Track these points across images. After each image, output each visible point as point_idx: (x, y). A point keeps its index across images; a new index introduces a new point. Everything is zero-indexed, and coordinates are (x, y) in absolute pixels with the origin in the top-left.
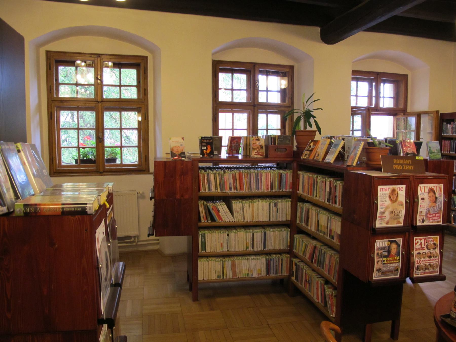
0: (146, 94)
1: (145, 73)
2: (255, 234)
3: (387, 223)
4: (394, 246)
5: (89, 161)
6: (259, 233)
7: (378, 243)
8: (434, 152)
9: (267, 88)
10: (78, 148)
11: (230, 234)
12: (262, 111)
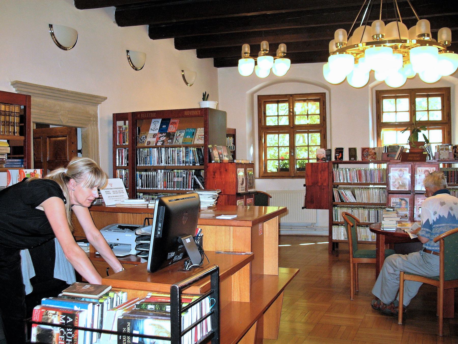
0: (325, 120)
2: (370, 211)
3: (398, 188)
4: (403, 202)
5: (287, 170)
6: (372, 212)
7: (393, 199)
11: (353, 211)
12: (317, 131)
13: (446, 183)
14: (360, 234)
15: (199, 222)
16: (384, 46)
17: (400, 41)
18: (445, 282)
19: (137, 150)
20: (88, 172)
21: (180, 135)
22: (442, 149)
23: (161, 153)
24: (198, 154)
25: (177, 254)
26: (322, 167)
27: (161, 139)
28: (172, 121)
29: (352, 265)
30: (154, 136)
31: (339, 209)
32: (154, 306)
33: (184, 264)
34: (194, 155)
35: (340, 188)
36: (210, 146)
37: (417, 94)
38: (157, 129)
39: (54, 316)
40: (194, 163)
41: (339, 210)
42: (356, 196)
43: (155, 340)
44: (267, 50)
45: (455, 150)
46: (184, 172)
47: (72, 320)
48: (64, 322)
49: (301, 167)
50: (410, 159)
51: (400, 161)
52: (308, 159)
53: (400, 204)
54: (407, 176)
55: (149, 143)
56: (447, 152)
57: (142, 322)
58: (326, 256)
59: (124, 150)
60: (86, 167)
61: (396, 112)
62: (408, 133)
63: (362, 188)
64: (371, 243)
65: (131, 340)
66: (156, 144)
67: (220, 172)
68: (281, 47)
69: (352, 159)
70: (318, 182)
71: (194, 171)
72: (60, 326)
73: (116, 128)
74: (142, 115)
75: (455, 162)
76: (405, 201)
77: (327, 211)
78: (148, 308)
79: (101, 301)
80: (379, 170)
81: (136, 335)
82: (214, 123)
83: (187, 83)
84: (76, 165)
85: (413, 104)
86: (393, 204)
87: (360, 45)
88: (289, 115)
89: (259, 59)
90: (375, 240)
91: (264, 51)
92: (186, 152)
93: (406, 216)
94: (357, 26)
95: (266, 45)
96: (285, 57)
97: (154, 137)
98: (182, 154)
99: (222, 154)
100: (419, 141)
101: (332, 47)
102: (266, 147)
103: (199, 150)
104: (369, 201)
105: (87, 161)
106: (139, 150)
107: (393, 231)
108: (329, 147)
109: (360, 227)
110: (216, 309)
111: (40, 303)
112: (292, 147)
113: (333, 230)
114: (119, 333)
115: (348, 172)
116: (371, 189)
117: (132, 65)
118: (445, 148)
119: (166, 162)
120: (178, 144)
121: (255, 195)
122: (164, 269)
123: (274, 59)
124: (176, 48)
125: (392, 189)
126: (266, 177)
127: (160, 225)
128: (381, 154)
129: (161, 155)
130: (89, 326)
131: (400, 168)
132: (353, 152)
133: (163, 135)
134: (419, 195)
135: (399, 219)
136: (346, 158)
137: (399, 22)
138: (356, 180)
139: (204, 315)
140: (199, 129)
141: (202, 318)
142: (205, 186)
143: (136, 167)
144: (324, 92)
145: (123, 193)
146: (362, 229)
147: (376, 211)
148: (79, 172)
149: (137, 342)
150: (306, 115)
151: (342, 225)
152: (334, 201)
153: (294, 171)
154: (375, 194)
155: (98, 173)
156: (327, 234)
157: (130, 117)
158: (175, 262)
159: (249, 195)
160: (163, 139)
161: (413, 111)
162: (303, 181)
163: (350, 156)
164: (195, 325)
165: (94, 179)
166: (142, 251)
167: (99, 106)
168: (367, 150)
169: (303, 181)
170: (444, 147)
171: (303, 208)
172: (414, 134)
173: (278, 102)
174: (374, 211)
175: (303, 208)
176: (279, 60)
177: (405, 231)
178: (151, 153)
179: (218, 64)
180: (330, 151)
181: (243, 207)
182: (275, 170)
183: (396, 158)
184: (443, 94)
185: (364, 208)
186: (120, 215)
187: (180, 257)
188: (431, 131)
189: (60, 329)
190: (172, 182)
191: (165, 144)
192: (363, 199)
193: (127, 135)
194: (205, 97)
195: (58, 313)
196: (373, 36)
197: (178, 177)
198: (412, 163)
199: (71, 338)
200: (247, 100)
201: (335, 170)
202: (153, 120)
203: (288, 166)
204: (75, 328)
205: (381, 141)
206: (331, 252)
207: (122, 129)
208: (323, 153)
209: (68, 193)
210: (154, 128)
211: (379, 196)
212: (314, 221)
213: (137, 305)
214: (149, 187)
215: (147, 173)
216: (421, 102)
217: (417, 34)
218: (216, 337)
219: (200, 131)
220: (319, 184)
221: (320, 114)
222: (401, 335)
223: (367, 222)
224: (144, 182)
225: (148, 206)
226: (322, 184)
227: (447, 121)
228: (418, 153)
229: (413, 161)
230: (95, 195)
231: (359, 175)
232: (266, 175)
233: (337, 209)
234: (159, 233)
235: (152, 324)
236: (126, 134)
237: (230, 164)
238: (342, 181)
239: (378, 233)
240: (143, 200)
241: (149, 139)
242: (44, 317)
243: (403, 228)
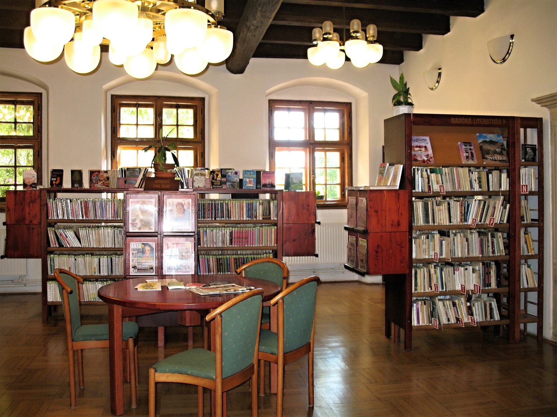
1: (39, 110)
2: (101, 259)
3: (140, 229)
4: (147, 248)
6: (104, 260)
8: (296, 183)
9: (15, 119)
11: (77, 259)
14: (87, 292)
26: (31, 197)
31: (57, 258)
42: (81, 239)
45: (213, 175)
51: (142, 189)
54: (153, 208)
56: (202, 178)
58: (38, 326)
62: (151, 153)
69: (75, 185)
70: (24, 219)
75: (211, 192)
76: (150, 246)
77: (39, 261)
85: (158, 115)
86: (133, 252)
93: (152, 268)
100: (167, 162)
104: (100, 245)
113: (48, 287)
115: (69, 205)
116: (102, 228)
118: (201, 173)
128: (116, 180)
131: (142, 200)
132: (77, 175)
136: (67, 184)
138: (81, 215)
144: (40, 92)
147: (109, 260)
150: (13, 123)
152: (49, 246)
161: (158, 125)
168: (96, 173)
184: (196, 106)
198: (160, 193)
201: (50, 202)
205: (117, 163)
211: (113, 238)
212: (23, 273)
216: (168, 115)
220: (27, 222)
226: (31, 221)
227: (200, 140)
228: (166, 178)
229: (160, 189)
231: (85, 208)
238: (60, 217)
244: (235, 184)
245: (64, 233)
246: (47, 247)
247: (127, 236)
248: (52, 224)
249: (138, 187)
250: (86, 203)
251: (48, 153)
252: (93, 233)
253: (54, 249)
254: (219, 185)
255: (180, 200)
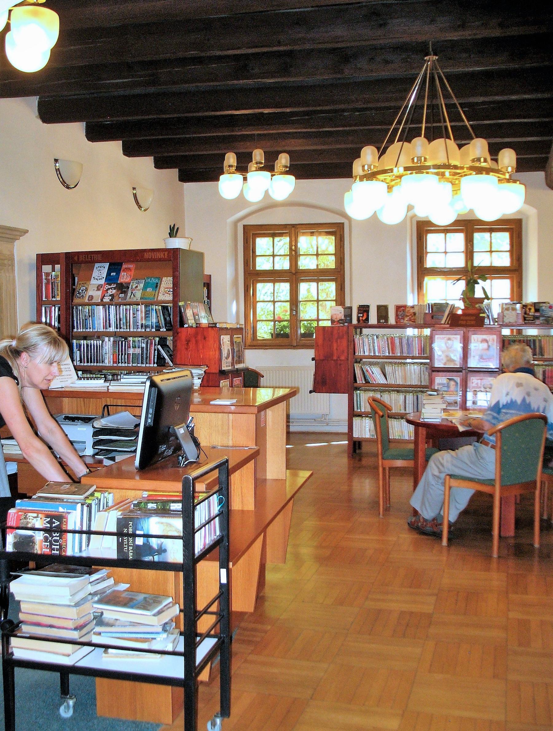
0: (343, 263)
1: (341, 241)
2: (407, 396)
4: (452, 383)
5: (286, 336)
6: (410, 397)
10: (274, 321)
13: (531, 356)
15: (192, 408)
16: (427, 173)
17: (447, 166)
18: (502, 487)
19: (73, 308)
20: (46, 343)
21: (137, 287)
22: (507, 309)
23: (109, 312)
24: (163, 315)
25: (169, 448)
27: (110, 292)
28: (124, 266)
29: (381, 469)
30: (99, 288)
32: (156, 504)
33: (178, 459)
34: (158, 317)
35: (365, 363)
36: (181, 304)
37: (475, 227)
38: (103, 278)
39: (35, 519)
40: (158, 328)
41: (363, 396)
43: (162, 540)
44: (261, 163)
46: (143, 341)
47: (59, 523)
48: (49, 525)
49: (307, 332)
50: (463, 323)
51: (448, 326)
52: (318, 320)
53: (448, 386)
54: (458, 346)
55: (91, 297)
56: (514, 312)
57: (146, 521)
58: (344, 461)
59: (53, 307)
60: (43, 337)
61: (446, 252)
62: (462, 285)
63: (395, 363)
64: (408, 442)
65: (134, 541)
66: (102, 300)
67: (197, 342)
68: (281, 158)
69: (381, 321)
70: (332, 355)
71: (157, 339)
72: (45, 530)
73: (42, 276)
74: (81, 257)
77: (346, 396)
78: (148, 507)
79: (88, 501)
80: (419, 337)
81: (140, 536)
82: (184, 268)
83: (140, 207)
84: (28, 335)
85: (469, 241)
87: (395, 170)
88: (290, 255)
89: (249, 175)
90: (413, 438)
91: (257, 163)
92: (146, 311)
93: (456, 403)
94: (391, 141)
95: (261, 154)
96: (287, 173)
97: (98, 289)
98: (141, 315)
99: (198, 315)
101: (357, 168)
102: (255, 302)
103: (165, 308)
104: (406, 382)
105: (43, 329)
106: (77, 308)
107: (437, 423)
108: (348, 304)
109: (393, 419)
110: (225, 510)
111: (14, 506)
112: (294, 302)
113: (354, 423)
114: (119, 534)
117: (61, 180)
119: (117, 325)
120: (135, 300)
121: (244, 373)
122: (154, 466)
123: (272, 175)
124: (124, 154)
125: (438, 364)
126: (254, 346)
127: (151, 411)
129: (109, 315)
130: (77, 529)
132: (382, 311)
133: (111, 287)
134: (474, 374)
135: (444, 406)
136: (373, 319)
137: (447, 140)
138: (387, 351)
139: (212, 515)
140: (164, 279)
141: (210, 518)
142: (174, 360)
143: (72, 333)
145: (70, 370)
146: (395, 422)
147: (415, 397)
148: (33, 344)
149: (142, 544)
151: (367, 417)
153: (297, 339)
154: (414, 373)
155: (58, 344)
156: (345, 430)
157: (63, 260)
158: (165, 457)
159: (236, 373)
160: (112, 292)
161: (469, 253)
162: (311, 353)
163: (379, 318)
164: (204, 526)
165: (54, 353)
166: (102, 450)
167: (17, 243)
168: (402, 308)
169: (311, 353)
170: (510, 306)
171: (311, 392)
172: (471, 284)
173: (273, 235)
174: (413, 396)
175: (311, 392)
176: (277, 177)
177: (453, 421)
178: (94, 314)
179: (185, 177)
180: (350, 310)
181: (228, 390)
182: (268, 337)
183: (443, 322)
185: (398, 391)
186: (66, 400)
187: (170, 452)
188: (495, 281)
189: (44, 534)
190: (125, 354)
191: (116, 300)
192: (396, 379)
193: (58, 286)
194: (173, 232)
195: (40, 515)
196: (413, 159)
197: (134, 347)
198: (465, 329)
199: (58, 544)
200: (229, 231)
201: (357, 338)
202: (97, 265)
203: (288, 331)
204: (62, 532)
205: (423, 295)
206: (350, 455)
207: (50, 278)
208: (340, 312)
209: (19, 372)
210: (99, 277)
212: (326, 411)
213: (135, 505)
214: (91, 362)
215: (89, 342)
217: (471, 158)
218: (225, 543)
219: (167, 282)
220: (335, 358)
221: (335, 254)
222: (445, 558)
223: (403, 411)
224: (84, 354)
225: (108, 389)
226: (339, 357)
230: (55, 373)
232: (255, 343)
233: (360, 394)
234: (149, 421)
235: (159, 523)
236: (56, 285)
237: (210, 329)
238: (366, 354)
239: (417, 425)
240: (102, 381)
241: (91, 293)
242: (22, 521)
243: (450, 418)
244: (550, 319)
245: (371, 370)
246: (354, 383)
247: (433, 371)
248: (359, 361)
249: (444, 324)
250: (392, 339)
251: (351, 284)
252: (399, 371)
253: (361, 385)
254: (533, 320)
255: (485, 337)
